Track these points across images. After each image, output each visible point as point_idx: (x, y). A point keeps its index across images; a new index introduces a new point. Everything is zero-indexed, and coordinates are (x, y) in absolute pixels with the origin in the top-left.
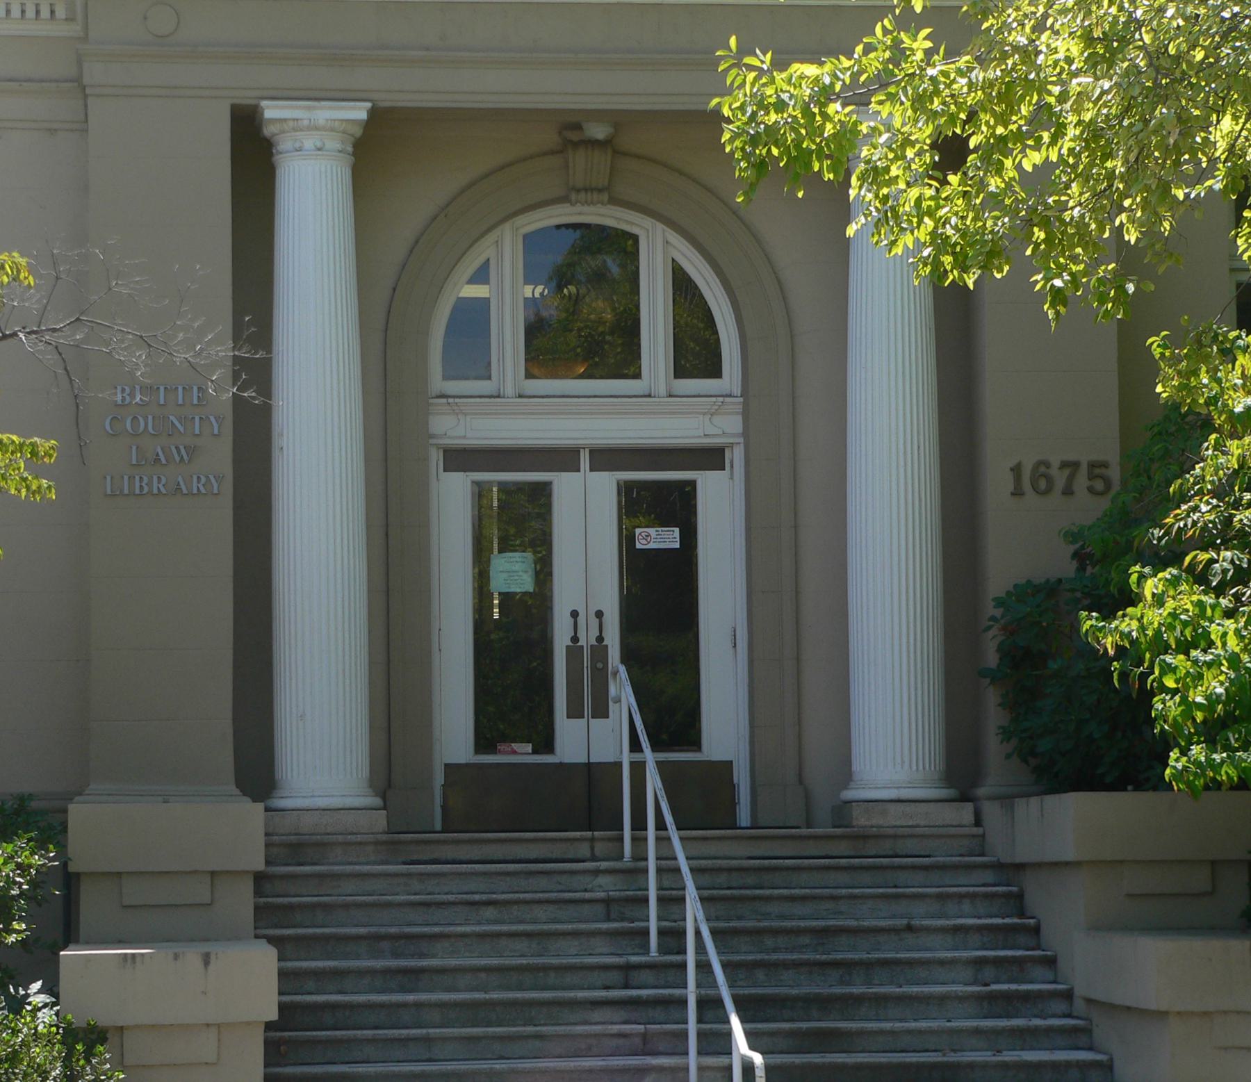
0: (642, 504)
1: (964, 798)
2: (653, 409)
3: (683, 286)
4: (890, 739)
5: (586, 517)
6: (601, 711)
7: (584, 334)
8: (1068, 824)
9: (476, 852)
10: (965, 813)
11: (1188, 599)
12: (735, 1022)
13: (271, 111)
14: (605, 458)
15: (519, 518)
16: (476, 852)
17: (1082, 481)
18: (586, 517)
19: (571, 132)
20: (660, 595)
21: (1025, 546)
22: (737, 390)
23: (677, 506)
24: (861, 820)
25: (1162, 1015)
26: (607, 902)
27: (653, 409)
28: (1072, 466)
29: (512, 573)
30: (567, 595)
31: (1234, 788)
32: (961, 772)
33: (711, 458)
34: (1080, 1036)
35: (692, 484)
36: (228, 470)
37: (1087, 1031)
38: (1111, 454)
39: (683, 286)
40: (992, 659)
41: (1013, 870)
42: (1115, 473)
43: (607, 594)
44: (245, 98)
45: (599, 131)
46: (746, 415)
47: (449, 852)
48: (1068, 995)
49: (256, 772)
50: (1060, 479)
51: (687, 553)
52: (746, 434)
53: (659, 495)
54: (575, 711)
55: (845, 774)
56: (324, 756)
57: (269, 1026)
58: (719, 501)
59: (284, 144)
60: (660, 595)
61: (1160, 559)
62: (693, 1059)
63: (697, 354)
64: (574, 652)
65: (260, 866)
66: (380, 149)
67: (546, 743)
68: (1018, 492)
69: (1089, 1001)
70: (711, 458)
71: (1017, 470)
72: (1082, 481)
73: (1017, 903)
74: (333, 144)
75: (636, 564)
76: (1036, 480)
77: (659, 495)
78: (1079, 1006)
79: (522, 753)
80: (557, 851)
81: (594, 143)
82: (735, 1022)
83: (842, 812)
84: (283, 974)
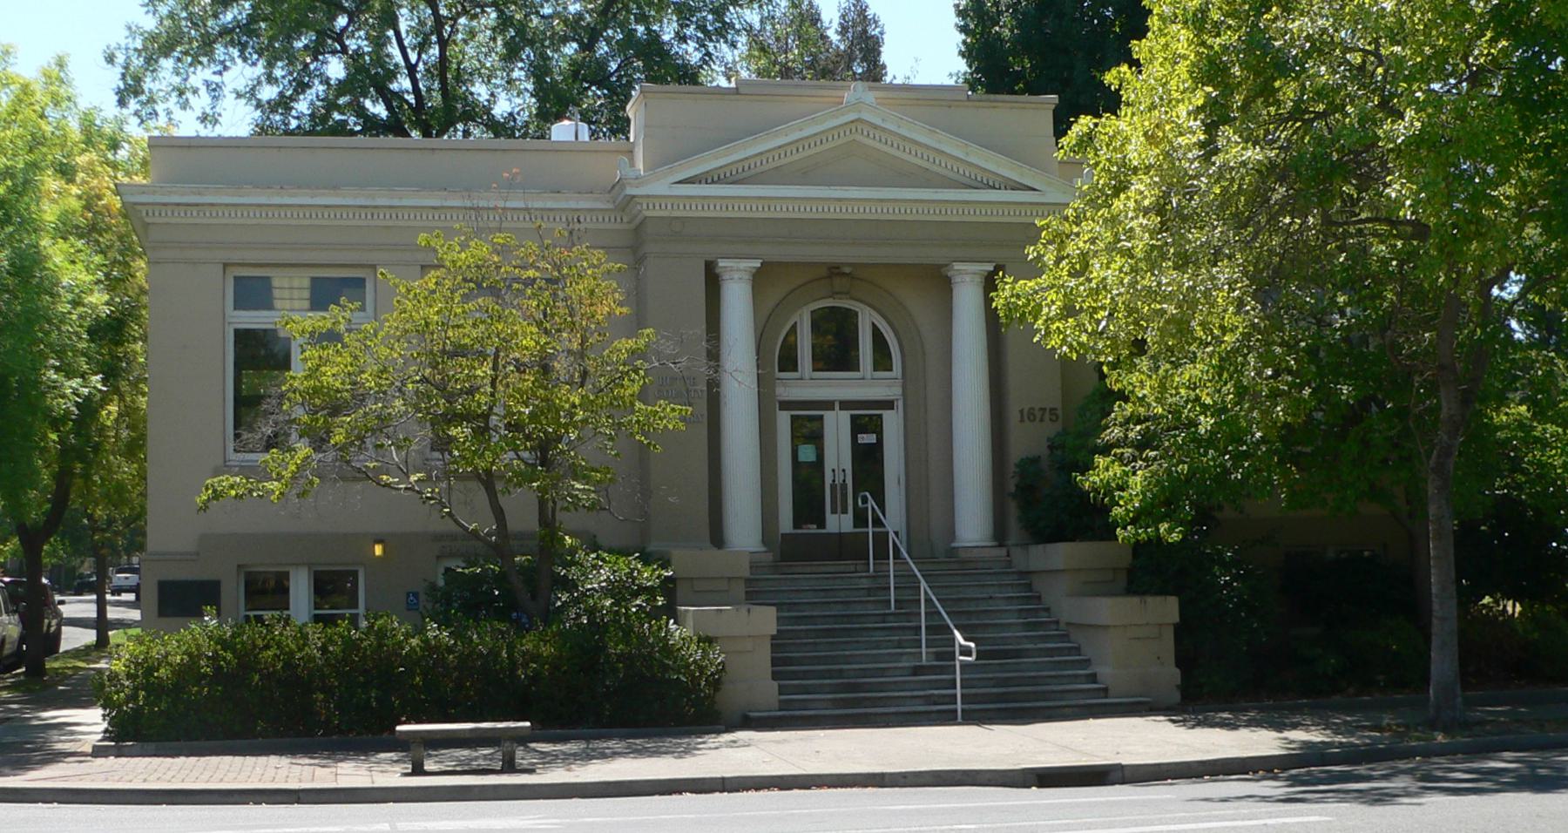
0: (858, 426)
1: (1001, 546)
2: (864, 384)
3: (878, 337)
4: (972, 521)
5: (837, 428)
6: (845, 511)
7: (837, 353)
8: (1061, 554)
9: (808, 570)
10: (1003, 551)
11: (1117, 469)
12: (957, 633)
13: (722, 263)
14: (845, 405)
15: (808, 430)
16: (808, 570)
17: (1047, 416)
18: (837, 428)
19: (834, 271)
20: (868, 461)
21: (1027, 441)
22: (900, 375)
23: (876, 426)
24: (962, 555)
25: (1106, 627)
26: (869, 589)
27: (864, 384)
28: (1043, 410)
29: (807, 453)
30: (830, 463)
31: (588, 509)
32: (1000, 533)
33: (889, 405)
34: (1065, 637)
35: (880, 416)
36: (705, 413)
37: (1067, 636)
38: (1059, 405)
39: (878, 337)
40: (1012, 489)
41: (1024, 574)
42: (1059, 412)
43: (847, 464)
44: (709, 258)
45: (847, 270)
46: (904, 388)
47: (799, 570)
48: (1057, 622)
49: (717, 537)
50: (1038, 415)
51: (879, 445)
52: (904, 394)
53: (866, 420)
54: (834, 511)
55: (951, 533)
56: (744, 528)
57: (773, 638)
58: (892, 423)
59: (726, 276)
60: (868, 461)
61: (1105, 450)
62: (924, 649)
63: (882, 358)
64: (833, 487)
65: (747, 574)
66: (760, 280)
67: (822, 524)
68: (1022, 420)
69: (1068, 624)
70: (889, 405)
71: (1021, 412)
72: (1047, 416)
73: (1029, 587)
74: (747, 276)
75: (856, 447)
76: (1029, 416)
77: (866, 420)
78: (1062, 626)
79: (812, 529)
80: (842, 568)
81: (844, 274)
82: (957, 633)
83: (952, 552)
84: (778, 618)
